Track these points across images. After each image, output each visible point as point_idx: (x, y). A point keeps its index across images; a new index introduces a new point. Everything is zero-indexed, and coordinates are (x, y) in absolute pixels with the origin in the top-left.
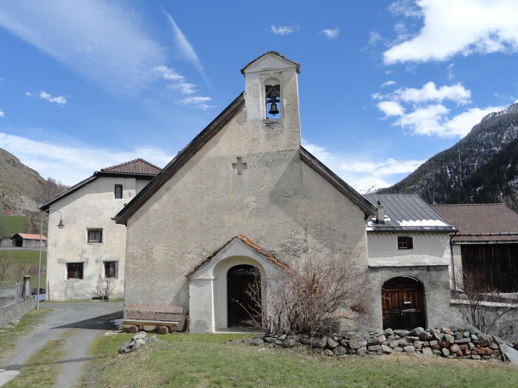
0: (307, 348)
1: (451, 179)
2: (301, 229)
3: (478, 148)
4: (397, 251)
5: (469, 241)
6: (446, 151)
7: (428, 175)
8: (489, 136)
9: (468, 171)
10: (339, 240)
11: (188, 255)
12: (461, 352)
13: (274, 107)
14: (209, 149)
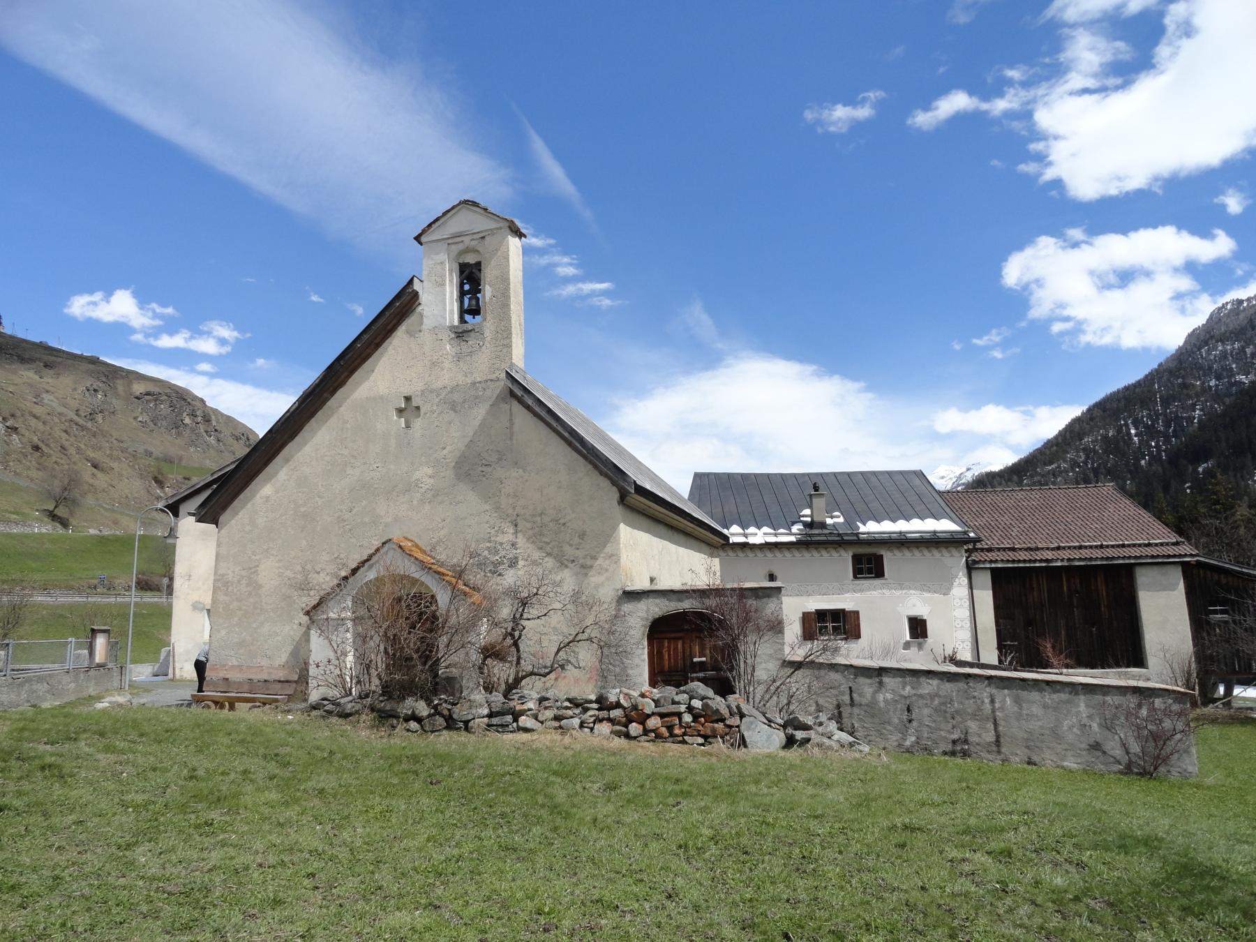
0: (374, 718)
1: (1139, 448)
2: (508, 524)
3: (1200, 380)
4: (849, 582)
5: (1008, 561)
6: (1127, 388)
7: (1088, 441)
8: (1226, 351)
9: (1178, 428)
10: (571, 542)
11: (316, 575)
12: (664, 730)
13: (474, 302)
14: (359, 384)
